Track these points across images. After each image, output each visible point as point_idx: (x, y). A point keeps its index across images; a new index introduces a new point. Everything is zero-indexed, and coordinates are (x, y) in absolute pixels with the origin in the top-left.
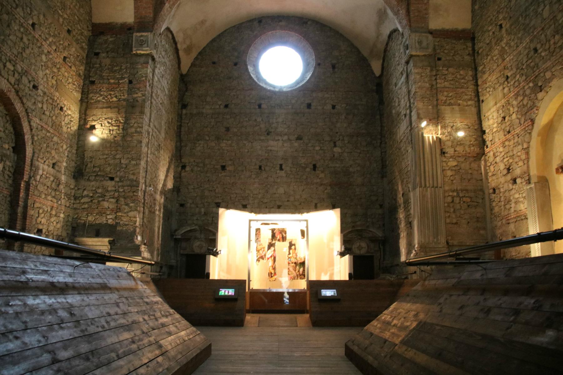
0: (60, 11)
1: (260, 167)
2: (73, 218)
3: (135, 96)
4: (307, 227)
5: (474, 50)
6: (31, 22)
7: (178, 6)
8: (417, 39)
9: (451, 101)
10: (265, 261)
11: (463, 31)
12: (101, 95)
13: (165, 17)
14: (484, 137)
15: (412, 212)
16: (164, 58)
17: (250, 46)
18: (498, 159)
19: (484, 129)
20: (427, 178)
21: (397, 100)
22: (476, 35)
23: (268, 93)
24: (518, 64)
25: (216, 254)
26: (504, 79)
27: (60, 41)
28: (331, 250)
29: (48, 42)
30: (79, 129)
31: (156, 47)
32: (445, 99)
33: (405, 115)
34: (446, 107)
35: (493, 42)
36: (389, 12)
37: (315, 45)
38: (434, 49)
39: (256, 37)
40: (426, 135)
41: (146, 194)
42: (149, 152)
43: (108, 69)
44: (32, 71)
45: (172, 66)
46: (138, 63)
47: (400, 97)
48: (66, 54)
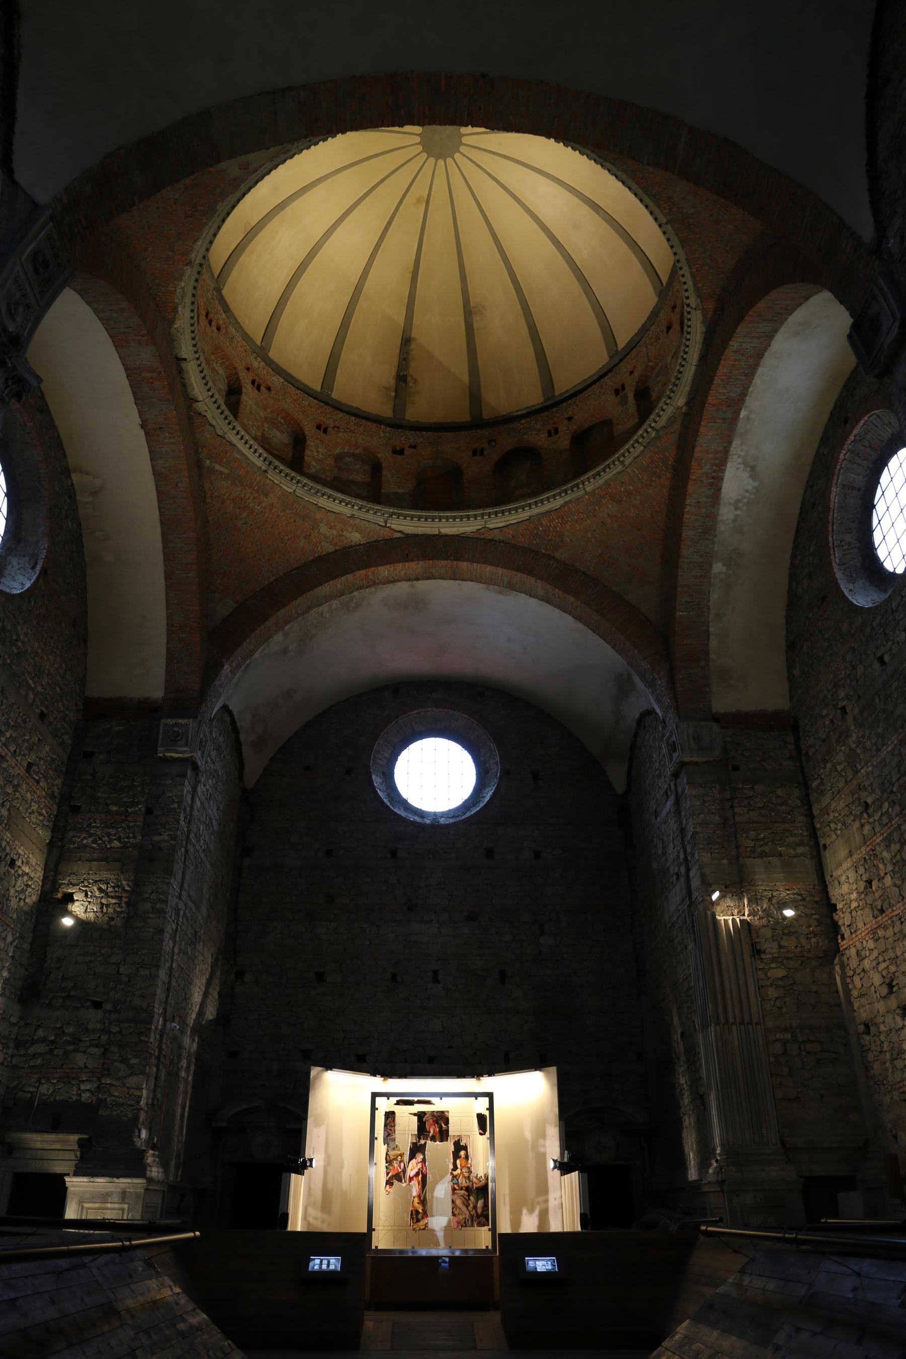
0: (31, 682)
1: (394, 977)
2: (8, 1088)
3: (158, 838)
4: (491, 1109)
5: (798, 748)
7: (247, 668)
9: (763, 848)
10: (404, 1185)
12: (91, 835)
14: (836, 917)
15: (704, 1074)
16: (214, 763)
18: (867, 964)
19: (833, 902)
20: (728, 996)
24: (883, 783)
25: (301, 1167)
27: (24, 735)
28: (541, 1159)
30: (40, 901)
31: (202, 745)
32: (751, 844)
33: (678, 875)
36: (636, 679)
40: (721, 918)
41: (165, 1037)
42: (176, 950)
47: (665, 838)
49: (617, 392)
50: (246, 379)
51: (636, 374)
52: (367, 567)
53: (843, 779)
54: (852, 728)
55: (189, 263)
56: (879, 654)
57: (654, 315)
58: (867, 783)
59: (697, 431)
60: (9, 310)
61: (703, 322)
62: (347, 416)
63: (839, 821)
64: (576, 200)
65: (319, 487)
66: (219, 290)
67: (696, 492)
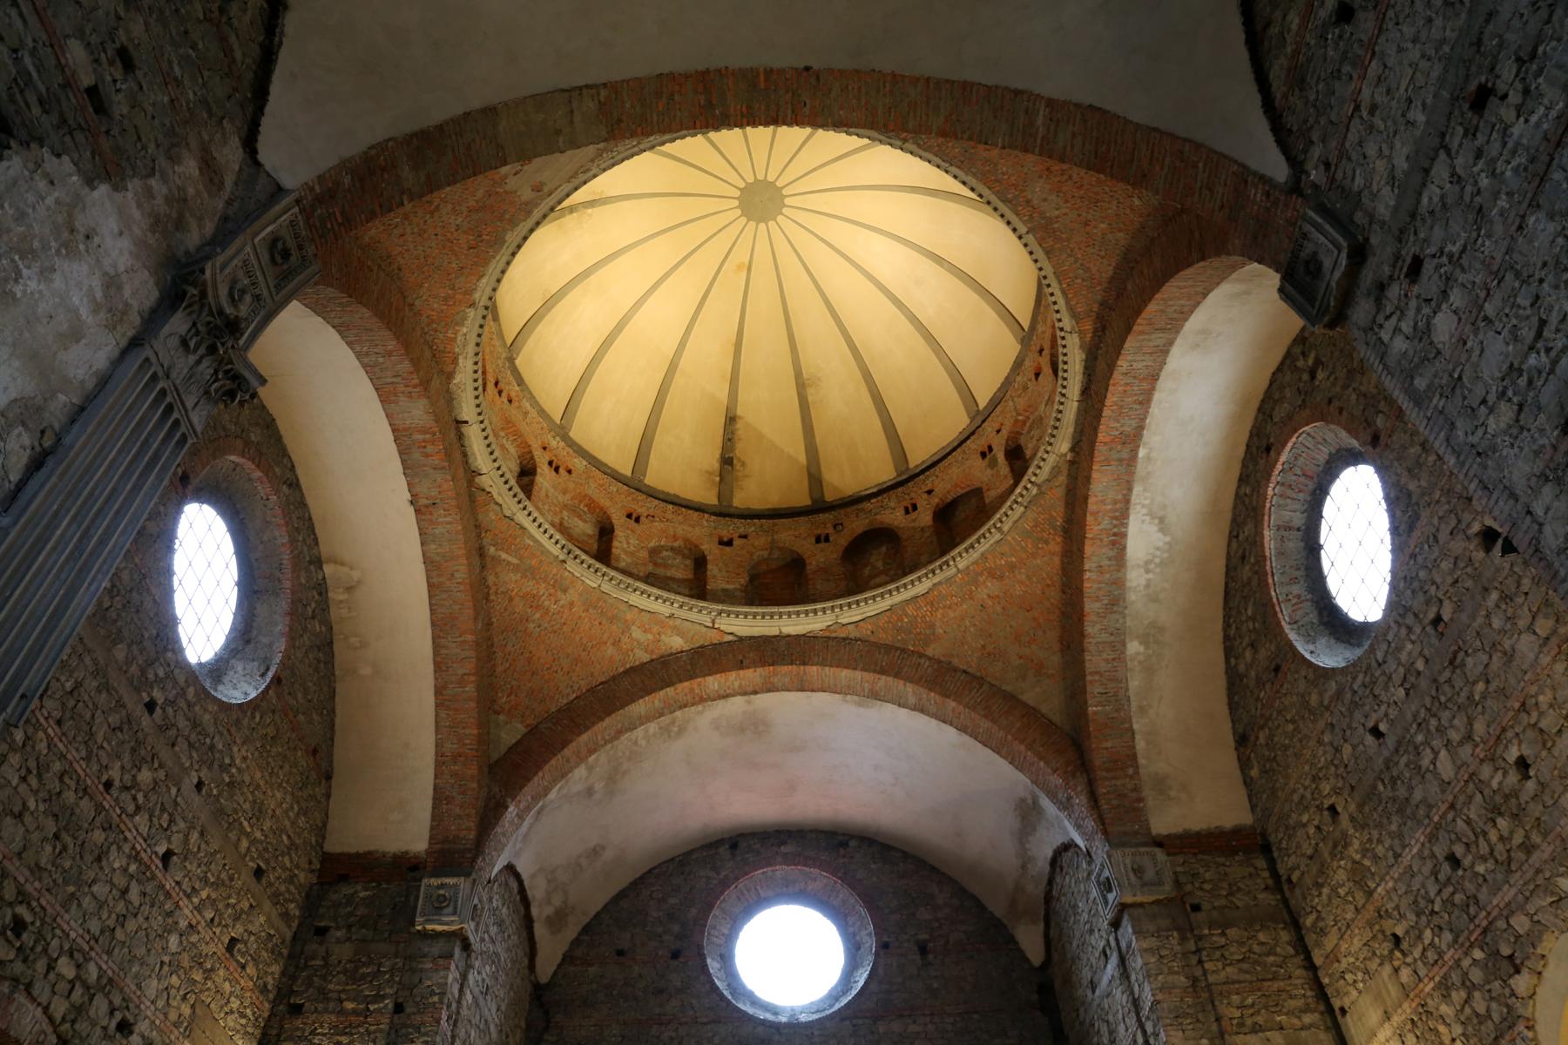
0: (246, 824)
6: (161, 850)
8: (1128, 861)
11: (1237, 831)
13: (503, 840)
17: (711, 906)
21: (1104, 1029)
22: (1272, 839)
23: (760, 1029)
24: (1415, 902)
26: (1387, 946)
27: (229, 897)
29: (196, 900)
31: (475, 913)
32: (1237, 1014)
34: (1248, 1037)
35: (1325, 850)
37: (871, 900)
38: (1177, 884)
39: (725, 884)
43: (345, 972)
44: (128, 981)
45: (514, 962)
46: (425, 956)
47: (1111, 1018)
48: (238, 931)
49: (983, 455)
50: (542, 461)
51: (1004, 432)
52: (691, 678)
53: (1352, 907)
54: (1351, 831)
55: (473, 305)
56: (1370, 724)
57: (1018, 365)
58: (1390, 906)
59: (1088, 479)
60: (231, 295)
61: (1081, 347)
62: (663, 504)
63: (1358, 968)
64: (915, 254)
65: (630, 581)
66: (511, 360)
67: (1095, 555)
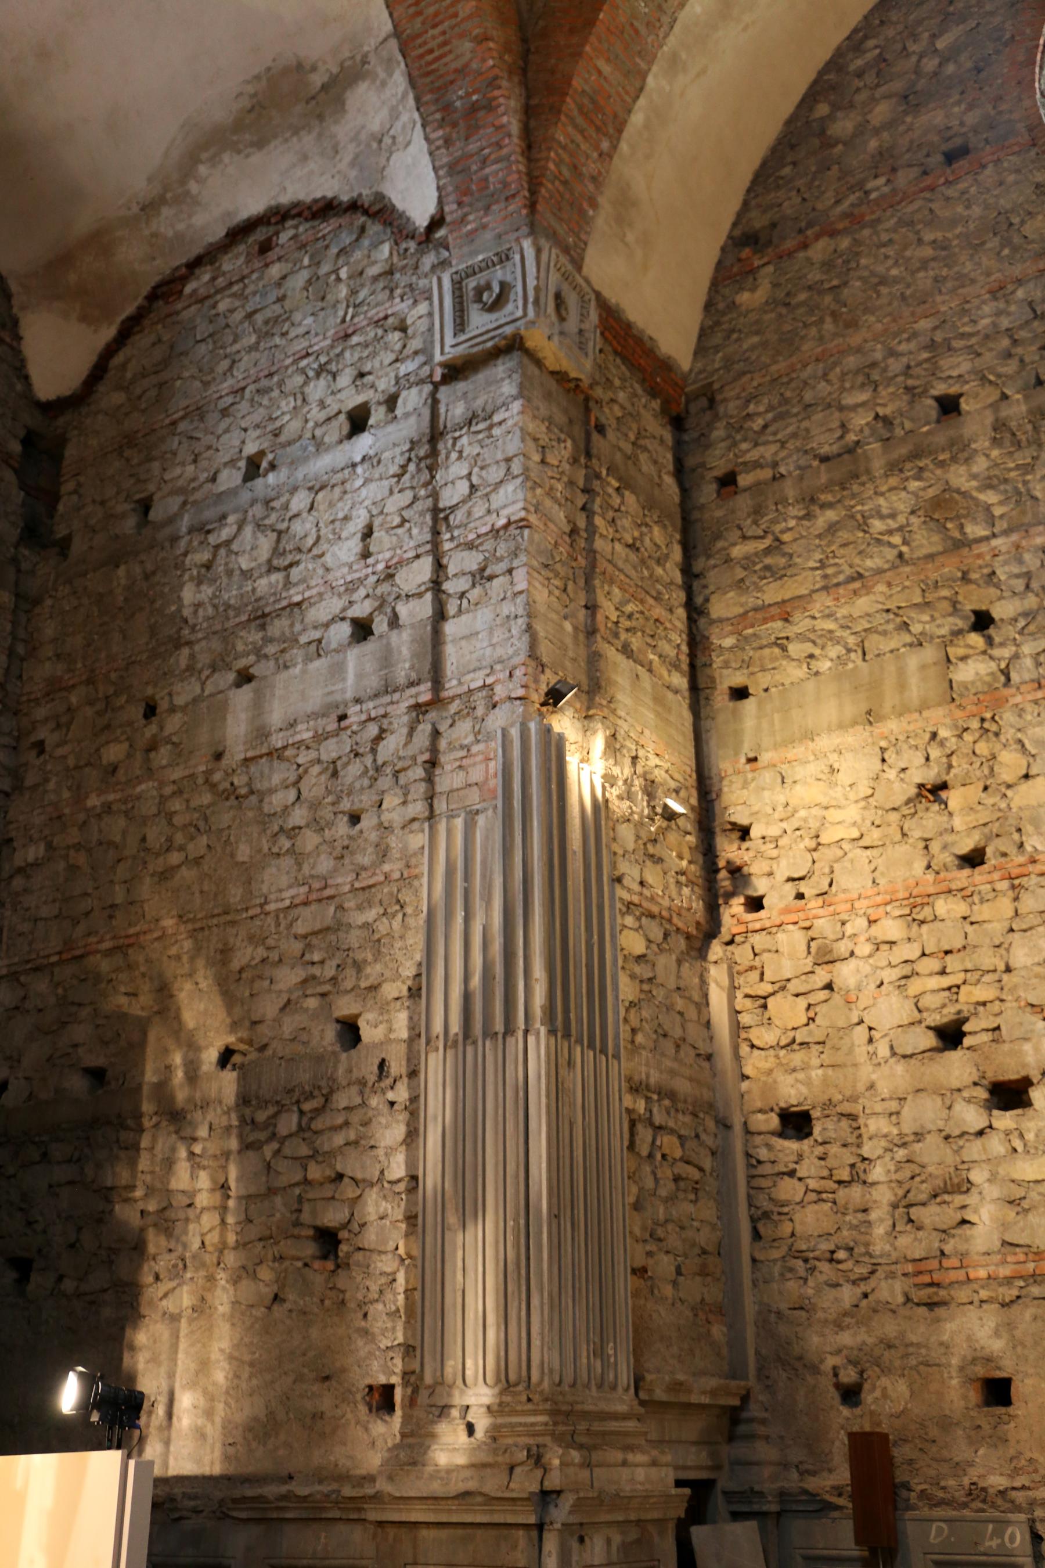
11: (666, 365)
